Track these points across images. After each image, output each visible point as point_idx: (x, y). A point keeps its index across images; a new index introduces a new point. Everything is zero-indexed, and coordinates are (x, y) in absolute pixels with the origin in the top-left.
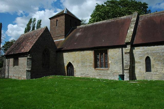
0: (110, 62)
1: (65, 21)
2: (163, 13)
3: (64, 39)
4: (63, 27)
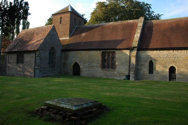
0: (117, 63)
1: (70, 20)
2: (187, 84)
3: (68, 38)
4: (68, 26)
